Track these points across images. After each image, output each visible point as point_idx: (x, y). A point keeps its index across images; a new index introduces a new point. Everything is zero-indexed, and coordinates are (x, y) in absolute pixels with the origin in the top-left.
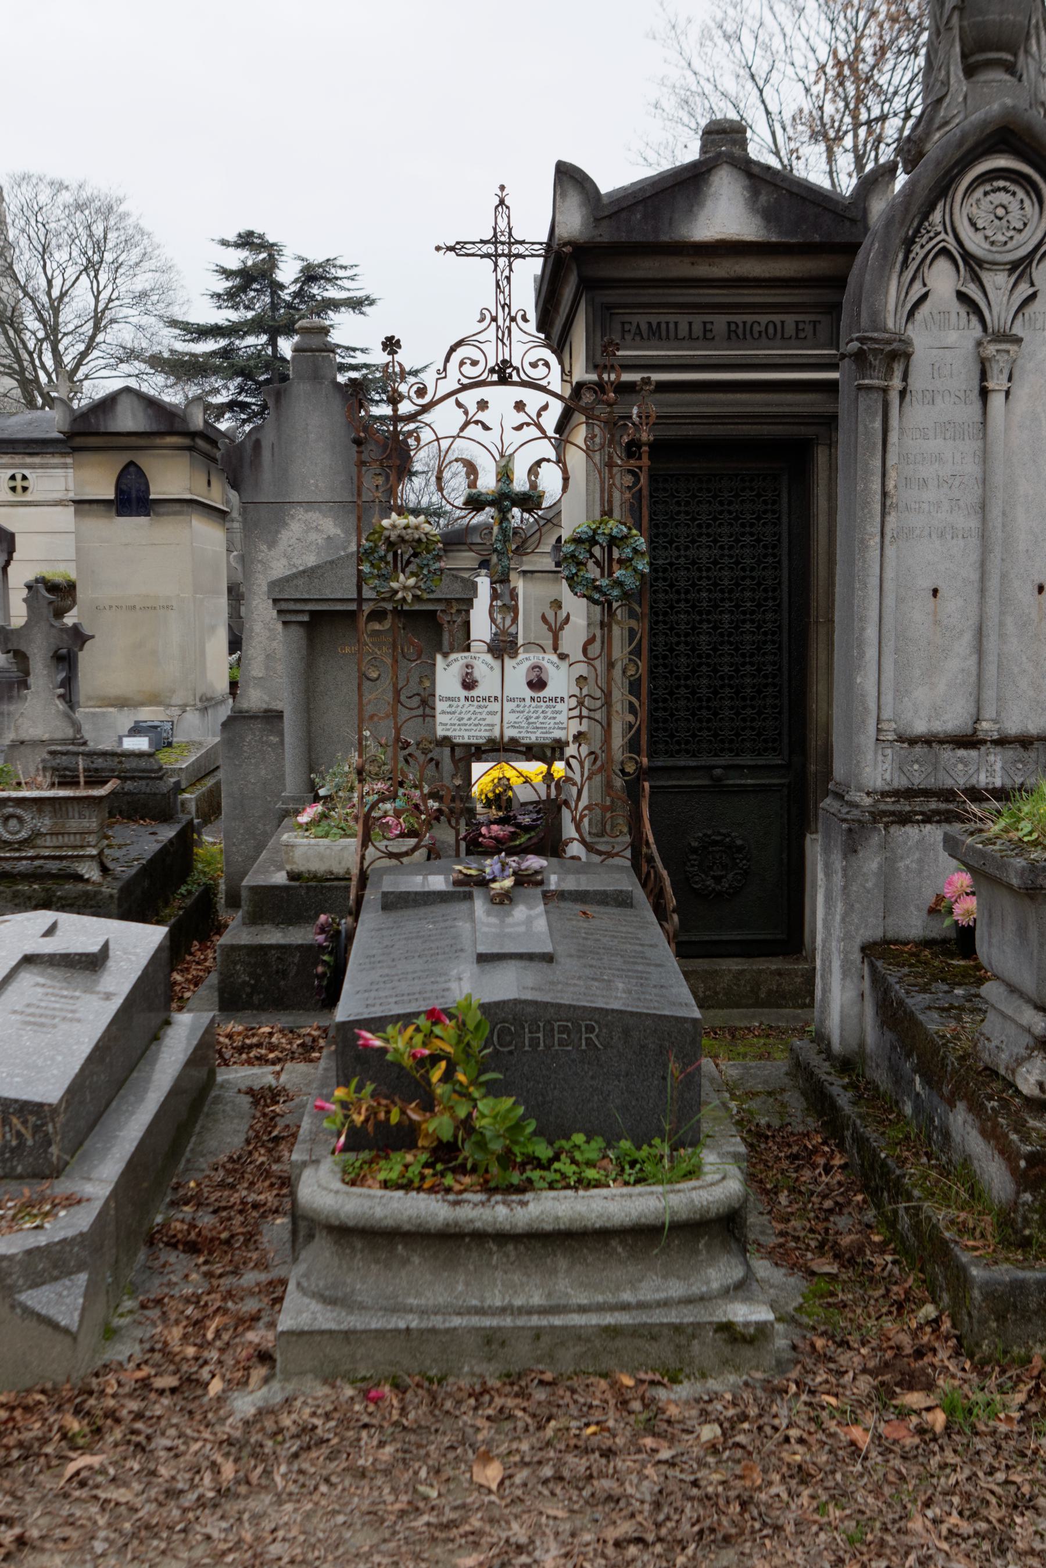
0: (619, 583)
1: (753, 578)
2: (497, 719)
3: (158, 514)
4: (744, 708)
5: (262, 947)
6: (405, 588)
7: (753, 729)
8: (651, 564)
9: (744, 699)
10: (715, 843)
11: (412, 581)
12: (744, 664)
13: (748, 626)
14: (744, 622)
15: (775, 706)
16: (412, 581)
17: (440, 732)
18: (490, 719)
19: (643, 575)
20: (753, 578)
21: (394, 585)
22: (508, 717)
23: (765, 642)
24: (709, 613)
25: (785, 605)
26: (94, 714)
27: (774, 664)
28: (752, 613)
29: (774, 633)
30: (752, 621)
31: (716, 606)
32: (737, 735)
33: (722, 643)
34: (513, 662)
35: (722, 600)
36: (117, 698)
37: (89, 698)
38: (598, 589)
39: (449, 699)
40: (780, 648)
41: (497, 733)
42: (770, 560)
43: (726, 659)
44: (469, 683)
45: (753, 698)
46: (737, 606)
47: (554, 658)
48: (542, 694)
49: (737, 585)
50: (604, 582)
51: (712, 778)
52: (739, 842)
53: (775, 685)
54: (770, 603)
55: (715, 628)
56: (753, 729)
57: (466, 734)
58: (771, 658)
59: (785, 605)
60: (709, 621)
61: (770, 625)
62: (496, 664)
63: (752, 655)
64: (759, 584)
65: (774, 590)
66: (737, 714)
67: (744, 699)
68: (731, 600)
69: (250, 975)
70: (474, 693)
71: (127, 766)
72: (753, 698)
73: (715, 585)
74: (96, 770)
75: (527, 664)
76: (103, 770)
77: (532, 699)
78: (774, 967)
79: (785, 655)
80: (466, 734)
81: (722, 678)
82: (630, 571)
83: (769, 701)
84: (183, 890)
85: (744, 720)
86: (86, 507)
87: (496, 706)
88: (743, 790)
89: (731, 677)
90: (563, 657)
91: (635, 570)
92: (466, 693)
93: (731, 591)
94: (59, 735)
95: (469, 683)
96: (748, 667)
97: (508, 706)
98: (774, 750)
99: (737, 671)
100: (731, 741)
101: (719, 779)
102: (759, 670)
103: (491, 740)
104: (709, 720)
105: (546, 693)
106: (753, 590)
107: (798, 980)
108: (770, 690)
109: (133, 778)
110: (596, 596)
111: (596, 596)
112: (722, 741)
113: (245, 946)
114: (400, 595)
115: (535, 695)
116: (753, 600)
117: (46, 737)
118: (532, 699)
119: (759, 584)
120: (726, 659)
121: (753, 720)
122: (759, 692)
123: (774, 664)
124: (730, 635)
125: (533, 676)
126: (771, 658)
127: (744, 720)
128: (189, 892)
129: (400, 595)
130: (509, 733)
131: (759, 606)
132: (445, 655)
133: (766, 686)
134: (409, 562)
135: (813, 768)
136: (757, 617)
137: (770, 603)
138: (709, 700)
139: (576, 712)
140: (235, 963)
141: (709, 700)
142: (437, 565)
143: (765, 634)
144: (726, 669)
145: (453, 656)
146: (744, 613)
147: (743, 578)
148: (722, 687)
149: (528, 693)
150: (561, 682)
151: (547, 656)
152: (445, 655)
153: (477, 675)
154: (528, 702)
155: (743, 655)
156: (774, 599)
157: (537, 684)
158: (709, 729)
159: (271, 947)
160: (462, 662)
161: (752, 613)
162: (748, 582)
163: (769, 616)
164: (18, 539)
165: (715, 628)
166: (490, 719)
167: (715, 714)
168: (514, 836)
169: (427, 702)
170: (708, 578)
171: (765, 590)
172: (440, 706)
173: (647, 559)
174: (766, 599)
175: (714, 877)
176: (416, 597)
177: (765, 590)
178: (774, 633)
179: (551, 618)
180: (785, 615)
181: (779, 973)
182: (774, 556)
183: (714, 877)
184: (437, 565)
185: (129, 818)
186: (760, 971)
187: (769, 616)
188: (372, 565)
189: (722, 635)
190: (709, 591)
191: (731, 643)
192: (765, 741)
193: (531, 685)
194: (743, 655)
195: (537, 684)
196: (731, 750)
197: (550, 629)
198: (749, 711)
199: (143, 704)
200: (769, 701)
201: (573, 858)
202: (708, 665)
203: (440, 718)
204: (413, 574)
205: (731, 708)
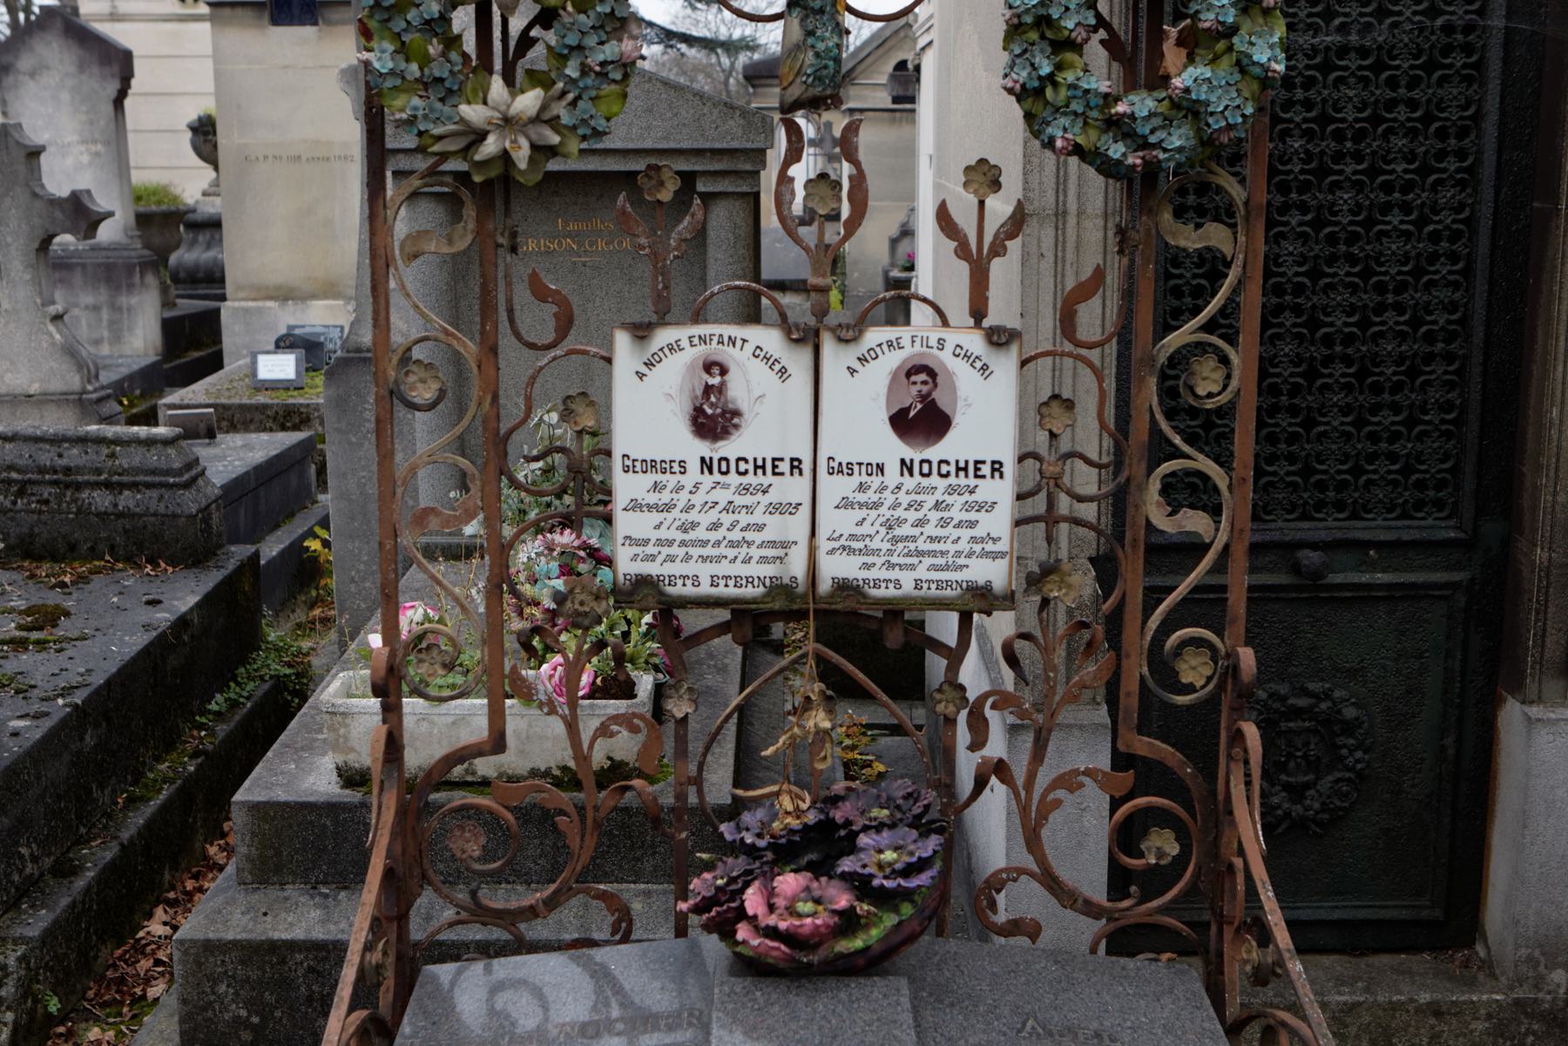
0: (1188, 109)
1: (1413, 105)
2: (797, 527)
3: (329, 23)
4: (1376, 408)
5: (274, 947)
6: (508, 122)
7: (1393, 457)
8: (1289, 49)
9: (1377, 389)
10: (1297, 713)
11: (529, 101)
12: (1380, 309)
13: (1395, 218)
14: (1386, 209)
15: (1448, 407)
16: (529, 101)
17: (627, 564)
18: (775, 528)
19: (1265, 81)
20: (1413, 105)
21: (473, 113)
22: (833, 521)
23: (1433, 258)
24: (1304, 187)
25: (1488, 171)
26: (246, 310)
27: (1452, 307)
28: (1408, 187)
29: (1455, 236)
30: (1406, 208)
31: (1323, 172)
32: (1357, 471)
33: (1332, 260)
34: (849, 356)
35: (1339, 157)
36: (278, 288)
37: (239, 288)
38: (1119, 126)
39: (651, 466)
40: (1467, 272)
41: (797, 567)
42: (1458, 60)
43: (1341, 297)
44: (712, 419)
45: (1397, 388)
46: (1373, 172)
47: (975, 342)
48: (935, 452)
49: (1376, 120)
50: (1140, 104)
51: (1296, 569)
52: (1350, 713)
53: (1449, 358)
54: (1452, 164)
55: (1318, 224)
56: (1393, 457)
57: (705, 571)
58: (1444, 294)
59: (1488, 171)
60: (1303, 208)
61: (1447, 218)
62: (798, 362)
63: (1401, 288)
64: (1427, 119)
65: (1463, 133)
66: (1359, 423)
67: (1377, 389)
68: (1358, 157)
69: (248, 1004)
70: (729, 449)
71: (125, 462)
72: (1397, 388)
73: (1324, 120)
74: (67, 470)
75: (892, 361)
76: (79, 470)
77: (906, 466)
78: (1425, 997)
79: (1481, 286)
80: (705, 571)
81: (1328, 341)
82: (1225, 70)
83: (1434, 394)
84: (217, 703)
85: (1374, 438)
86: (227, 11)
87: (794, 488)
88: (1364, 596)
89: (1349, 340)
90: (999, 338)
91: (1243, 65)
92: (703, 448)
93: (1360, 136)
94: (56, 386)
95: (712, 419)
96: (1390, 316)
97: (833, 488)
98: (1439, 504)
99: (1365, 324)
100: (1342, 486)
101: (1317, 575)
102: (1415, 323)
103: (780, 589)
104: (1293, 438)
105: (949, 448)
106: (1412, 133)
107: (1480, 1026)
108: (1439, 368)
109: (134, 486)
110: (1116, 150)
111: (1116, 150)
112: (1321, 486)
113: (235, 944)
114: (491, 146)
115: (908, 452)
116: (1410, 157)
117: (35, 388)
118: (906, 466)
119: (1427, 119)
120: (1341, 297)
121: (1394, 437)
122: (1413, 373)
123: (1452, 307)
124: (1353, 238)
125: (909, 397)
126: (1444, 294)
127: (1374, 438)
128: (234, 705)
129: (491, 146)
130: (835, 568)
131: (1425, 170)
132: (641, 332)
133: (1429, 358)
134: (526, 42)
135: (1540, 555)
136: (1422, 197)
137: (1452, 164)
138: (1295, 391)
139: (1038, 505)
140: (215, 981)
141: (1295, 391)
142: (610, 51)
143: (1435, 237)
144: (1340, 320)
145: (664, 336)
146: (1387, 188)
147: (1391, 105)
148: (1328, 361)
149: (893, 449)
150: (988, 412)
151: (952, 338)
152: (641, 332)
153: (738, 391)
154: (893, 474)
155: (1381, 288)
156: (1461, 154)
157: (922, 419)
158: (1292, 458)
159: (293, 946)
160: (691, 354)
161: (1408, 187)
162: (1402, 113)
163: (1447, 195)
164: (138, 66)
165: (1318, 224)
166: (775, 528)
167: (1309, 424)
168: (848, 922)
169: (583, 490)
170: (1308, 105)
171: (1442, 134)
172: (626, 487)
173: (1280, 31)
174: (1441, 155)
175: (1287, 787)
176: (541, 151)
177: (1442, 134)
178: (1455, 236)
179: (965, 219)
180: (1487, 192)
181: (1436, 1010)
182: (1468, 49)
183: (1287, 787)
184: (610, 51)
185: (130, 560)
186: (1394, 1007)
187: (1447, 195)
188: (403, 50)
189: (1332, 239)
190: (1309, 135)
191: (1352, 260)
192: (1420, 485)
193: (901, 423)
194: (1381, 288)
195: (922, 419)
196: (1340, 506)
197: (963, 251)
198: (1387, 418)
199: (314, 297)
200: (1434, 394)
201: (1015, 928)
202: (1297, 310)
203: (625, 523)
204: (537, 79)
205: (1346, 410)
